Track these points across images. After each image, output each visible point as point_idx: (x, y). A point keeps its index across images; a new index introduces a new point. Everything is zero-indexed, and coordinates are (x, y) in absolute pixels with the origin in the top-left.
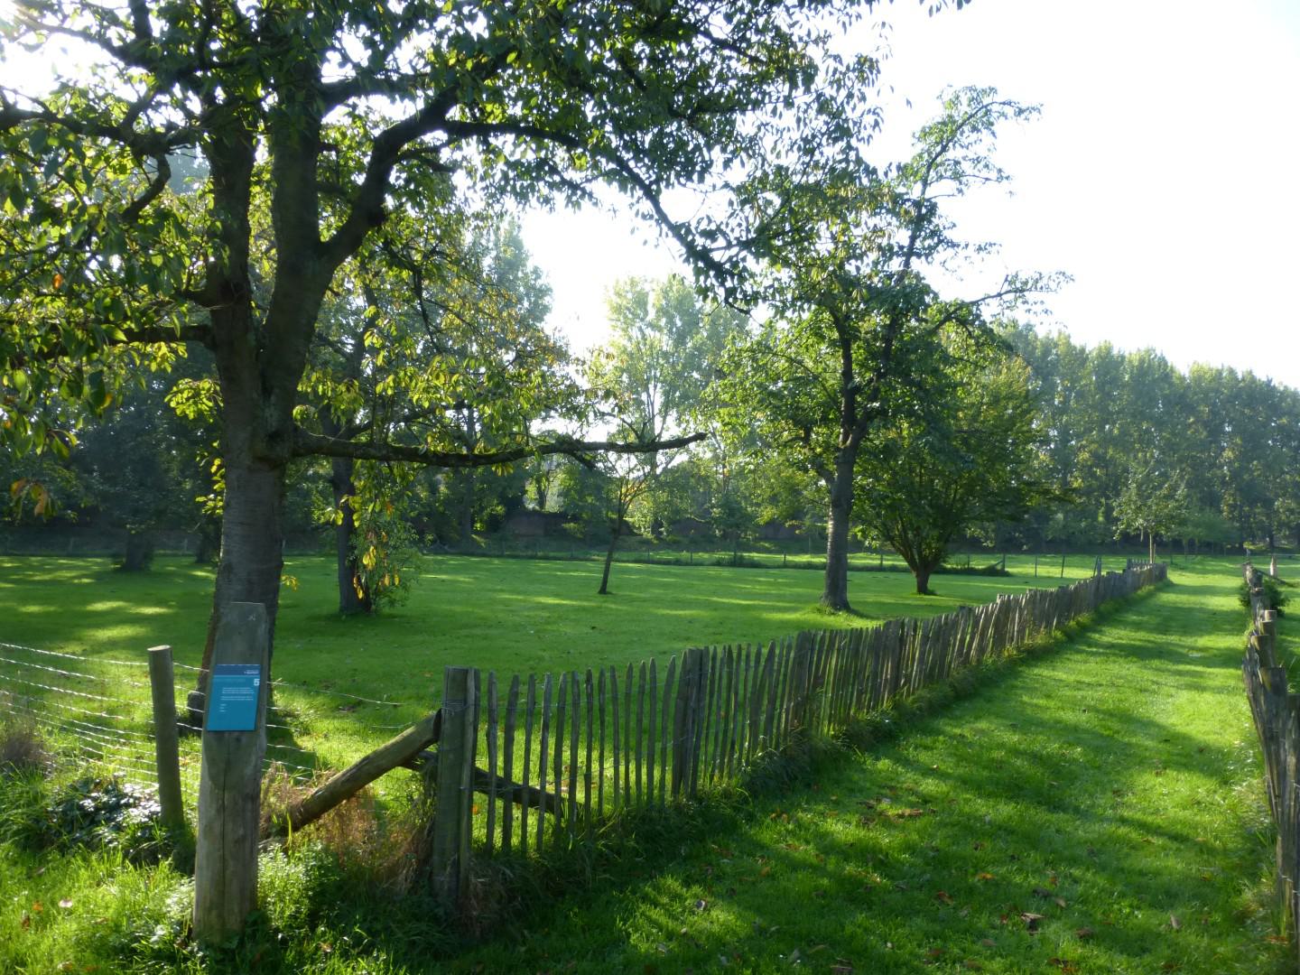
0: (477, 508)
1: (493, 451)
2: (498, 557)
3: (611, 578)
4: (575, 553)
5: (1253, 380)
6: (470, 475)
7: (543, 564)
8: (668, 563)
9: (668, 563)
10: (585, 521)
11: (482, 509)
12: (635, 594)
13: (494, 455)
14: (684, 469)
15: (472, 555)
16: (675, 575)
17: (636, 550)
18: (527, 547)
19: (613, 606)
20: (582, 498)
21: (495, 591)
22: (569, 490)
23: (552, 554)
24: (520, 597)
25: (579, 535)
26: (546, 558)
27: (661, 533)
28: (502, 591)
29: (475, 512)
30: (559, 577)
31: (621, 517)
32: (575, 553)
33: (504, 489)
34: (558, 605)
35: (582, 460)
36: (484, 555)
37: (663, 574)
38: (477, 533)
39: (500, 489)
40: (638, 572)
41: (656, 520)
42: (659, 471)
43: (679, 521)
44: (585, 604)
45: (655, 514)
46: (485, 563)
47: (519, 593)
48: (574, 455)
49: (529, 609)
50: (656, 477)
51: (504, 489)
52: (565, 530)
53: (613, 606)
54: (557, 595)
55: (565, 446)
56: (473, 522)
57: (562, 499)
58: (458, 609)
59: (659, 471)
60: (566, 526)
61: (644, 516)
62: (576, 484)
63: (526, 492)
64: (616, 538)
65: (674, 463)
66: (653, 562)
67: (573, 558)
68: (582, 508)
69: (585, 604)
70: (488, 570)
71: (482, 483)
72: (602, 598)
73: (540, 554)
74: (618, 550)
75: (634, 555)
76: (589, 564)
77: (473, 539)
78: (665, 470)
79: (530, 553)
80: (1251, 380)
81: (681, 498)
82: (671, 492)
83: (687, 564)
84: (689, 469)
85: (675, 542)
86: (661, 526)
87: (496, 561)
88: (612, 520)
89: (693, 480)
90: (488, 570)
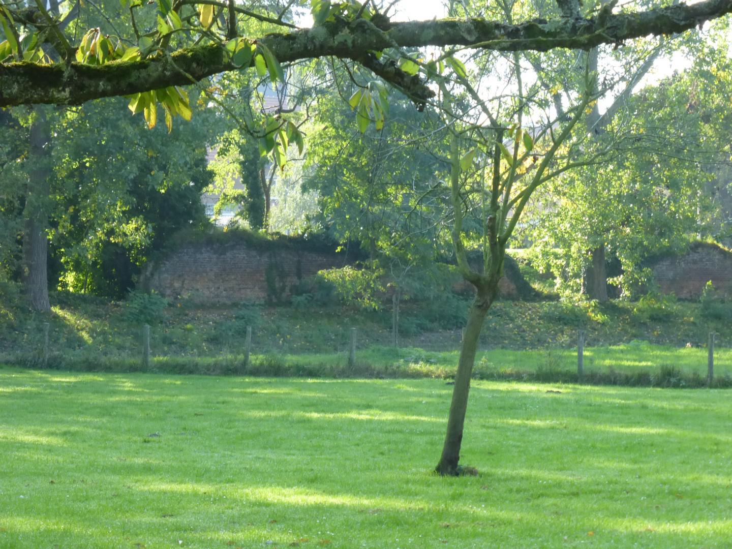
0: (65, 226)
1: (131, 54)
2: (131, 370)
3: (471, 428)
4: (360, 356)
5: (307, 504)
6: (42, 130)
7: (266, 389)
8: (640, 380)
9: (640, 380)
10: (386, 262)
11: (80, 231)
12: (547, 475)
13: (134, 66)
14: (682, 98)
15: (54, 365)
16: (664, 417)
17: (539, 342)
18: (214, 340)
19: (482, 511)
20: (375, 191)
21: (130, 470)
22: (336, 171)
23: (291, 359)
24: (203, 488)
25: (367, 302)
26: (276, 371)
27: (614, 291)
28: (148, 470)
29: (62, 241)
30: (319, 427)
31: (498, 245)
32: (360, 356)
33: (145, 169)
34: (319, 509)
35: (395, 77)
36: (90, 367)
37: (623, 414)
38: (66, 300)
39: (132, 170)
40: (554, 407)
41: (598, 253)
42: (604, 105)
43: (668, 254)
44: (399, 504)
45: (596, 234)
46: (96, 389)
47: (200, 476)
48: (370, 63)
49: (233, 523)
50: (597, 125)
51: (145, 169)
52: (327, 287)
53: (482, 511)
54: (312, 481)
55: (344, 35)
56: (55, 269)
57: (315, 196)
58: (658, 353)
59: (604, 105)
60: (331, 275)
61: (563, 241)
62: (358, 151)
63: (208, 177)
64: (483, 308)
65: (651, 80)
66: (595, 379)
67: (352, 370)
68: (374, 224)
69: (399, 504)
70: (106, 411)
71: (77, 154)
72: (445, 486)
73: (256, 359)
74: (485, 342)
75: (537, 358)
76: (403, 385)
77: (56, 317)
78: (623, 101)
79: (226, 357)
80: (316, 504)
81: (673, 185)
82: (644, 167)
83: (697, 383)
84: (695, 90)
85: (660, 318)
86: (615, 268)
87: (127, 383)
88: (475, 258)
89: (707, 129)
90: (106, 411)
